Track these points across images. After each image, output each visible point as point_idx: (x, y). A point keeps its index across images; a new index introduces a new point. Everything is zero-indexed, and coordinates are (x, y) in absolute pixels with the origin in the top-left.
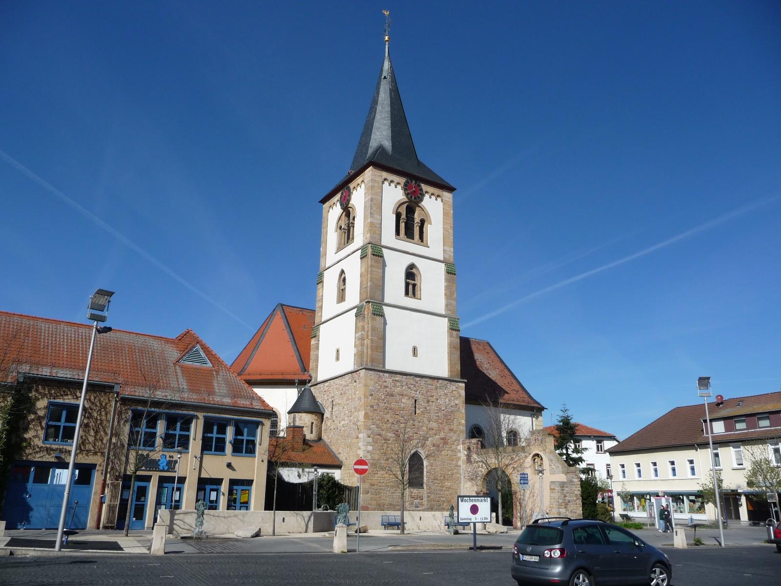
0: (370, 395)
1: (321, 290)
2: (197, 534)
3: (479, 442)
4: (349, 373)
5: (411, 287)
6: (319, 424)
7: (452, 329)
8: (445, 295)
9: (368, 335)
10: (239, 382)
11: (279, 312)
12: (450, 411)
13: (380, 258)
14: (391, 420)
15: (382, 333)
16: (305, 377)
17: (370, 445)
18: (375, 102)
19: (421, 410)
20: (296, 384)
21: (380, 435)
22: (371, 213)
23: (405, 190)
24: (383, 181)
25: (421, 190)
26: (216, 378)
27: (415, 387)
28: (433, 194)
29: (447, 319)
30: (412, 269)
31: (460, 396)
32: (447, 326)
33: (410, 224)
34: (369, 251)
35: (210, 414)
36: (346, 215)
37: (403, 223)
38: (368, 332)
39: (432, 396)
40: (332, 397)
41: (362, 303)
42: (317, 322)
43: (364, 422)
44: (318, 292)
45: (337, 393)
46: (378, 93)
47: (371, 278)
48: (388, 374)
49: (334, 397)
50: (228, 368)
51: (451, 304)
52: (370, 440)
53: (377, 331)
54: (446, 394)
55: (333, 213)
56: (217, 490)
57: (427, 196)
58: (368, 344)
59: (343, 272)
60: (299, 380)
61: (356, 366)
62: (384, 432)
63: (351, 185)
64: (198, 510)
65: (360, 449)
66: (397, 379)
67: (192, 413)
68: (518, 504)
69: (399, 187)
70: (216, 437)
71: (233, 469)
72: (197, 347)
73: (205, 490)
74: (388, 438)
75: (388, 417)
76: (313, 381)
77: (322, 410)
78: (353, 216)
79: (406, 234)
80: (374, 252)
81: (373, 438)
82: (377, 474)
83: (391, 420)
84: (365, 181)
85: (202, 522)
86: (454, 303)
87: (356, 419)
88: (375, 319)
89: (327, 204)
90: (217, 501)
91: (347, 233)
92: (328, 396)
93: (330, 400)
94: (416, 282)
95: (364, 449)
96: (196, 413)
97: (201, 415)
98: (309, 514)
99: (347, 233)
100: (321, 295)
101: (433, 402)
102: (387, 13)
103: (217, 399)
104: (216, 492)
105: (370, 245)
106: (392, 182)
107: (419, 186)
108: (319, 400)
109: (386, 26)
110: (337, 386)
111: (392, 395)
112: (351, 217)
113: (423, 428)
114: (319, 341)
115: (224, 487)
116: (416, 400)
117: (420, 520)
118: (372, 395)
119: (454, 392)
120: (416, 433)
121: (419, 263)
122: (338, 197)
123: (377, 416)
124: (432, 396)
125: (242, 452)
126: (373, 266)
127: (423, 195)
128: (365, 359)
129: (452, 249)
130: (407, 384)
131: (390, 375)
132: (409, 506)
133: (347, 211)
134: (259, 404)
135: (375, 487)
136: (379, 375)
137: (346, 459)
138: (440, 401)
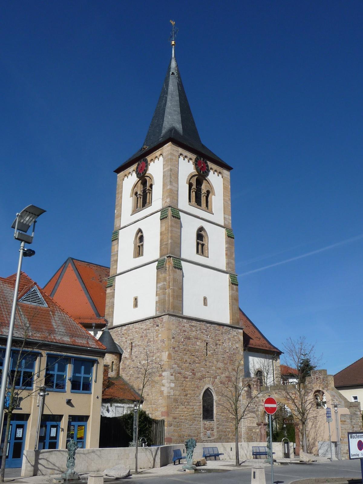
0: (172, 338)
1: (116, 246)
2: (70, 476)
3: (259, 380)
4: (150, 319)
5: (200, 246)
6: (118, 363)
7: (233, 284)
8: (226, 255)
9: (169, 286)
10: (73, 322)
11: (70, 265)
12: (232, 353)
13: (178, 220)
14: (189, 361)
15: (182, 284)
16: (102, 321)
17: (173, 383)
18: (165, 92)
19: (211, 351)
20: (94, 328)
21: (180, 373)
22: (170, 181)
23: (196, 165)
24: (179, 156)
25: (207, 166)
26: (53, 318)
27: (206, 332)
28: (216, 171)
29: (228, 275)
30: (201, 232)
31: (239, 341)
32: (228, 281)
33: (199, 194)
34: (170, 213)
35: (52, 352)
36: (141, 183)
37: (194, 193)
38: (169, 282)
39: (219, 340)
40: (131, 340)
41: (163, 258)
42: (112, 274)
43: (168, 361)
44: (113, 247)
45: (137, 335)
46: (167, 85)
47: (171, 236)
48: (186, 320)
49: (133, 339)
50: (61, 309)
51: (231, 263)
52: (173, 378)
53: (178, 282)
54: (229, 339)
55: (129, 181)
56: (57, 427)
57: (211, 172)
58: (169, 293)
59: (140, 231)
60: (96, 324)
61: (158, 312)
62: (183, 371)
63: (149, 158)
64: (69, 450)
65: (163, 385)
66: (193, 324)
67: (36, 350)
68: (300, 434)
69: (191, 162)
70: (57, 375)
71: (72, 406)
72: (35, 288)
73: (46, 427)
74: (187, 376)
75: (186, 358)
76: (109, 325)
77: (119, 350)
78: (150, 183)
79: (196, 201)
80: (171, 215)
81: (175, 376)
82: (179, 408)
83: (189, 361)
84: (164, 154)
85: (74, 462)
86: (233, 262)
87: (158, 359)
88: (175, 272)
89: (122, 174)
90: (56, 438)
91: (143, 198)
92: (126, 338)
93: (129, 342)
94: (204, 242)
95: (168, 386)
96: (40, 351)
97: (44, 353)
98: (156, 449)
99: (143, 198)
100: (116, 250)
101: (220, 345)
102: (173, 23)
103: (58, 338)
104: (56, 428)
105: (170, 208)
106: (186, 157)
107: (206, 163)
108: (116, 342)
109: (172, 33)
110: (137, 329)
111: (189, 338)
112: (148, 185)
113: (213, 368)
114: (114, 290)
115: (64, 424)
116: (207, 343)
117: (231, 450)
118: (173, 338)
119: (235, 337)
120: (207, 372)
121: (208, 227)
122: (134, 167)
123: (178, 357)
124: (219, 340)
125: (79, 389)
126: (173, 227)
127: (209, 171)
128: (167, 306)
129: (230, 218)
130: (200, 329)
131: (188, 321)
132: (203, 437)
133: (144, 179)
134: (94, 344)
135: (177, 420)
136: (179, 320)
137: (148, 395)
138: (225, 345)
